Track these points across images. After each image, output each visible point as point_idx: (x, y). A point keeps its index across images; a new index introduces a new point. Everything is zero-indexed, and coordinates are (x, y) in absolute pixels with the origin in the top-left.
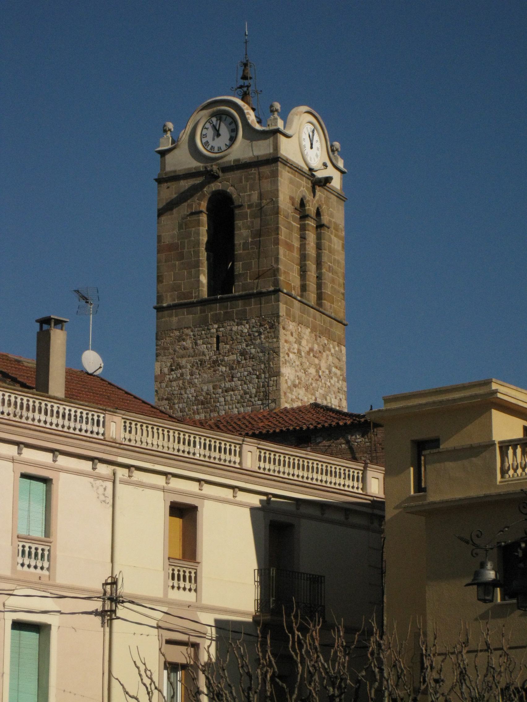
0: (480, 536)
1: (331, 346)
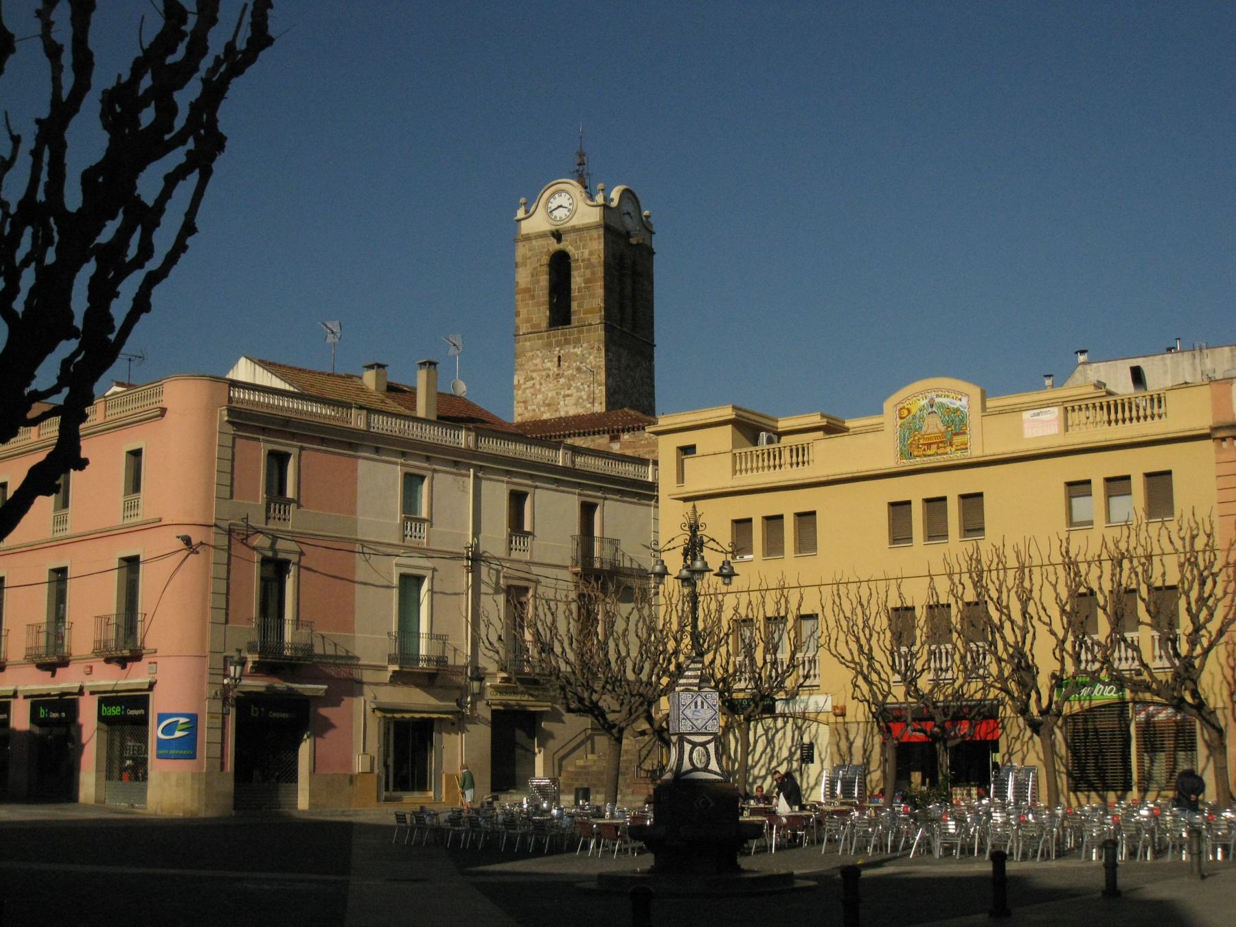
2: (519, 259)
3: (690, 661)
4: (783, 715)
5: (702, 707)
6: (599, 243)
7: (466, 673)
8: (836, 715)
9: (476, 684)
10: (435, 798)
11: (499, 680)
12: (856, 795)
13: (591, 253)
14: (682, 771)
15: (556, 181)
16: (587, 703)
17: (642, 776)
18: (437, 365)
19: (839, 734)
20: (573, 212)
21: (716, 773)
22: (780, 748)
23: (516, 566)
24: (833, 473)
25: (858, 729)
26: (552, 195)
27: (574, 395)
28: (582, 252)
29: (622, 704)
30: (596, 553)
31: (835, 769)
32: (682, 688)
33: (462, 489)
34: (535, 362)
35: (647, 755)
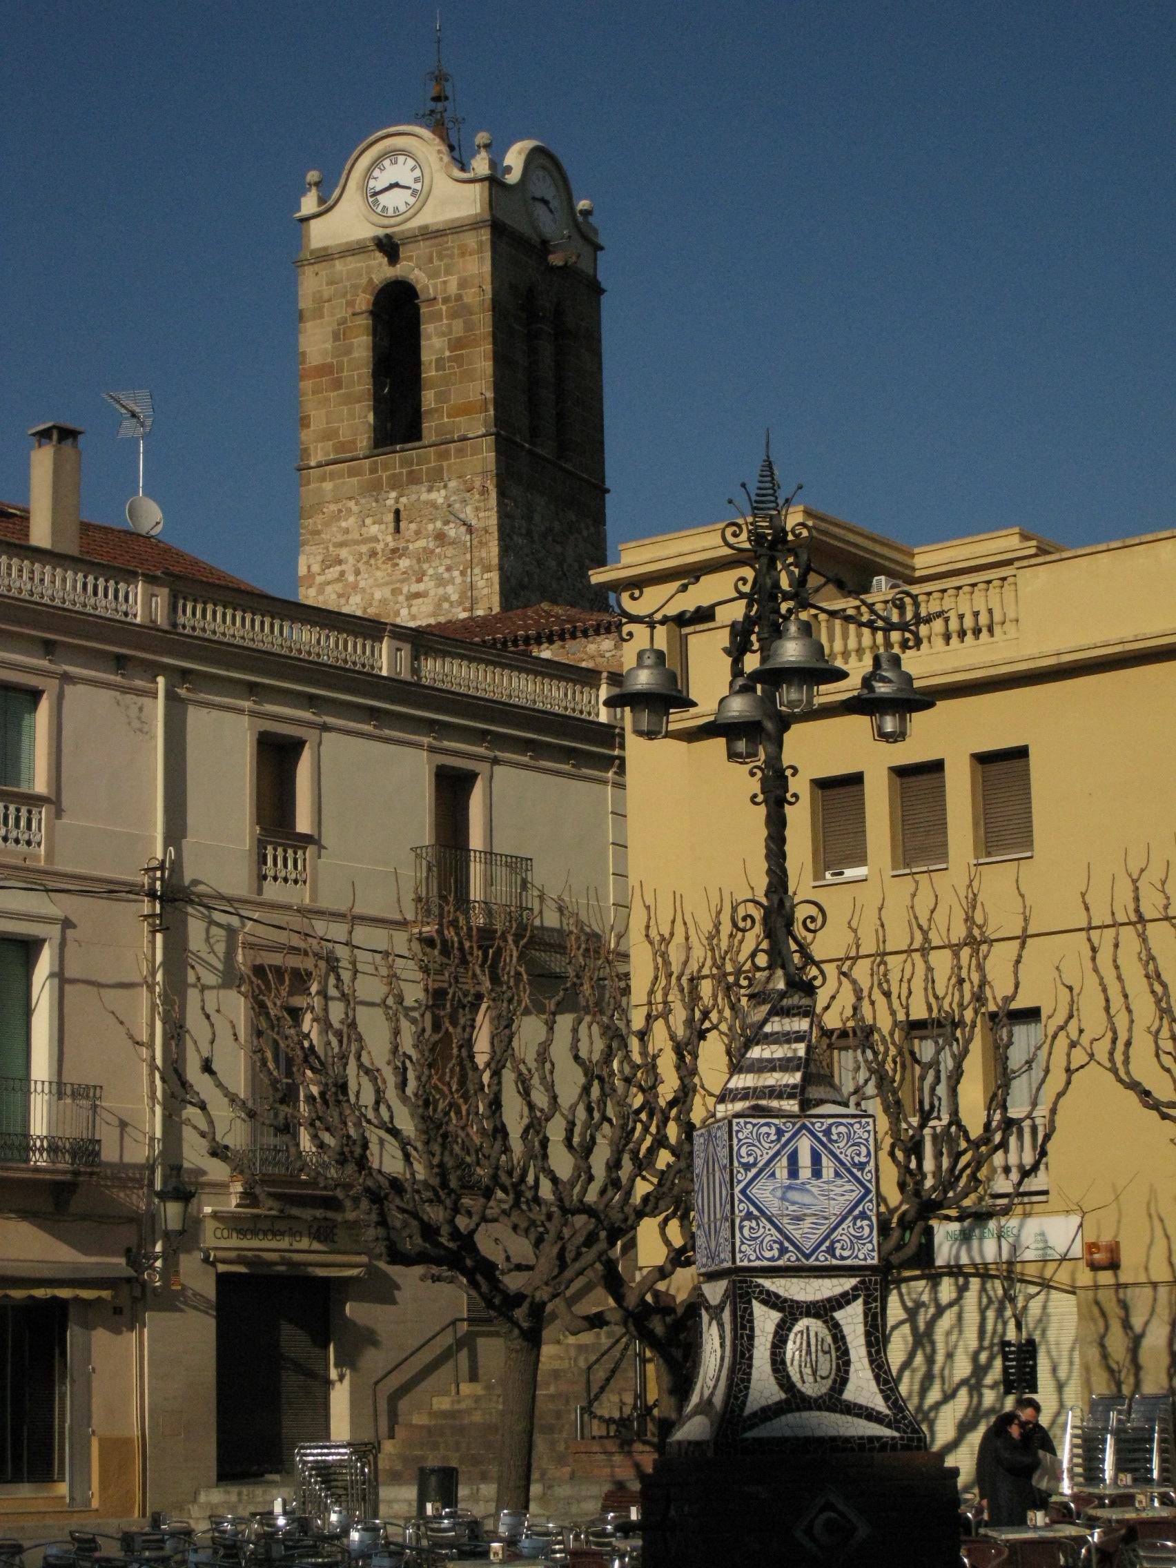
0: (740, 583)
1: (582, 525)
2: (305, 303)
3: (766, 1008)
4: (955, 1271)
5: (817, 1173)
6: (481, 260)
7: (151, 1183)
8: (1094, 1267)
9: (172, 1212)
10: (72, 1499)
11: (234, 1201)
12: (1155, 1475)
13: (463, 284)
14: (747, 1411)
15: (380, 134)
16: (444, 1240)
17: (596, 1432)
18: (80, 437)
19: (1104, 1314)
20: (422, 197)
21: (871, 1415)
22: (950, 1356)
23: (277, 918)
24: (1073, 645)
25: (1155, 1300)
26: (376, 163)
27: (432, 593)
28: (445, 282)
29: (538, 1242)
30: (476, 892)
31: (1098, 1407)
32: (739, 1106)
33: (136, 724)
34: (344, 524)
35: (608, 1380)
